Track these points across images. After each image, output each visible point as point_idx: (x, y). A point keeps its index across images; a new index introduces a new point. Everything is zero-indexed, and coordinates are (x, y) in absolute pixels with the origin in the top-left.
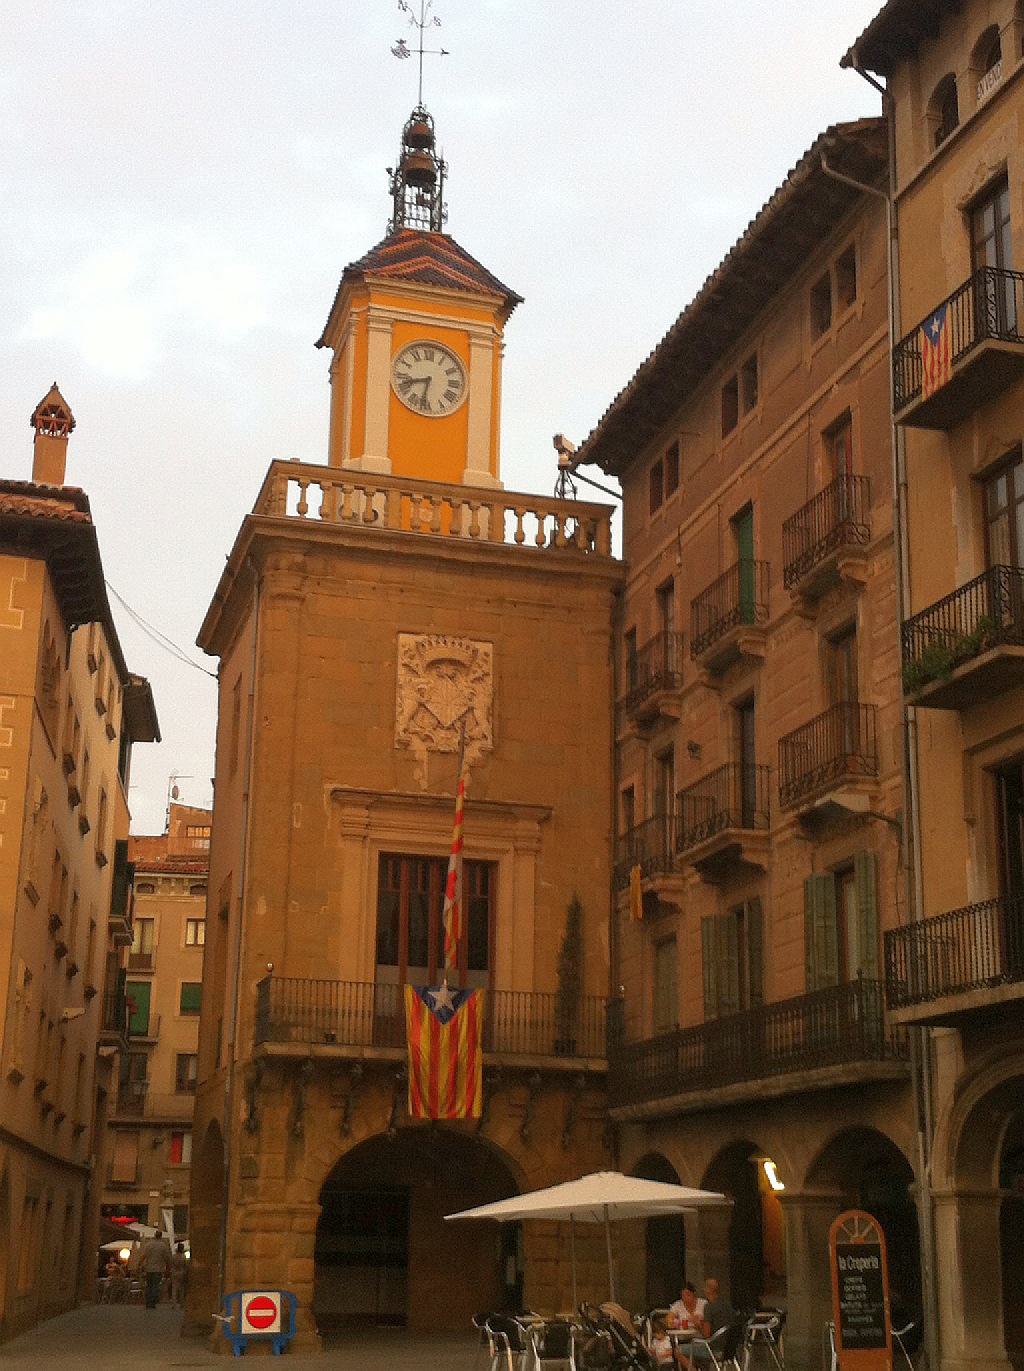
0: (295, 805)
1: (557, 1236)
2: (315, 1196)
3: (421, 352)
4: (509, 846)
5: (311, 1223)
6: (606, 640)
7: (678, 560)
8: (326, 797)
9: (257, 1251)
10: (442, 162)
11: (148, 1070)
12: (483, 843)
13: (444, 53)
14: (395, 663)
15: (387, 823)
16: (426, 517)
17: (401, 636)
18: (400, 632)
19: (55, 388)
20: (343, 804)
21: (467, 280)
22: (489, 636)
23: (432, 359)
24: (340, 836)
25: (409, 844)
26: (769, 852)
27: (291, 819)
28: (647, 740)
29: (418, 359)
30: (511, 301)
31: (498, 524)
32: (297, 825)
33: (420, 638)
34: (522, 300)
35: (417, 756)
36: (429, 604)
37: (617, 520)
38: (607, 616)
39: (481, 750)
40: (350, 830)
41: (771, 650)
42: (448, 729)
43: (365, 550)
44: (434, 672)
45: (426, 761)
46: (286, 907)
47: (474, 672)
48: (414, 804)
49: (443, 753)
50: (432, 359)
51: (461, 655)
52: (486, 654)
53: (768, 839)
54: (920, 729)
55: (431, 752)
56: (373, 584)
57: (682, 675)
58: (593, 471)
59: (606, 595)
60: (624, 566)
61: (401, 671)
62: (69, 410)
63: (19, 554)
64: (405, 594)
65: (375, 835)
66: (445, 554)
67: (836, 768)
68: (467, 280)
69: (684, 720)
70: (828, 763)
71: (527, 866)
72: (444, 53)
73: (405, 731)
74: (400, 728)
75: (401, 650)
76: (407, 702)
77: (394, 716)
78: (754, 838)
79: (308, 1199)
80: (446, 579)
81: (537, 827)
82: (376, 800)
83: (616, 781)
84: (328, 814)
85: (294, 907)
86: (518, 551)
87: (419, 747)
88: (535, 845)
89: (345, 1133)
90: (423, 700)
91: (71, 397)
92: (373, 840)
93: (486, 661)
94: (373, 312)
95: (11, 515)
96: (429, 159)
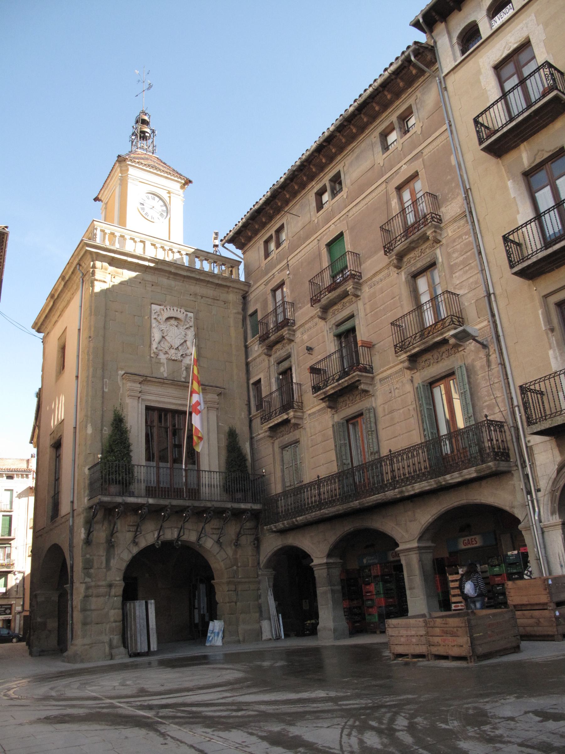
0: (105, 380)
1: (235, 591)
2: (122, 577)
6: (241, 317)
7: (288, 272)
11: (314, 146)
17: (153, 305)
18: (152, 304)
22: (192, 310)
25: (159, 402)
27: (103, 388)
28: (270, 356)
33: (162, 307)
35: (162, 361)
36: (165, 293)
37: (242, 267)
38: (241, 306)
40: (132, 394)
46: (102, 430)
48: (162, 382)
49: (174, 360)
51: (180, 316)
54: (498, 297)
55: (169, 360)
56: (139, 281)
58: (231, 246)
60: (247, 284)
61: (153, 321)
65: (144, 397)
66: (173, 270)
67: (421, 336)
70: (416, 334)
73: (156, 348)
74: (154, 346)
75: (153, 312)
76: (157, 336)
77: (151, 342)
79: (118, 579)
81: (217, 397)
82: (145, 380)
83: (248, 379)
84: (121, 386)
85: (105, 430)
87: (162, 357)
88: (217, 406)
89: (135, 542)
93: (191, 321)
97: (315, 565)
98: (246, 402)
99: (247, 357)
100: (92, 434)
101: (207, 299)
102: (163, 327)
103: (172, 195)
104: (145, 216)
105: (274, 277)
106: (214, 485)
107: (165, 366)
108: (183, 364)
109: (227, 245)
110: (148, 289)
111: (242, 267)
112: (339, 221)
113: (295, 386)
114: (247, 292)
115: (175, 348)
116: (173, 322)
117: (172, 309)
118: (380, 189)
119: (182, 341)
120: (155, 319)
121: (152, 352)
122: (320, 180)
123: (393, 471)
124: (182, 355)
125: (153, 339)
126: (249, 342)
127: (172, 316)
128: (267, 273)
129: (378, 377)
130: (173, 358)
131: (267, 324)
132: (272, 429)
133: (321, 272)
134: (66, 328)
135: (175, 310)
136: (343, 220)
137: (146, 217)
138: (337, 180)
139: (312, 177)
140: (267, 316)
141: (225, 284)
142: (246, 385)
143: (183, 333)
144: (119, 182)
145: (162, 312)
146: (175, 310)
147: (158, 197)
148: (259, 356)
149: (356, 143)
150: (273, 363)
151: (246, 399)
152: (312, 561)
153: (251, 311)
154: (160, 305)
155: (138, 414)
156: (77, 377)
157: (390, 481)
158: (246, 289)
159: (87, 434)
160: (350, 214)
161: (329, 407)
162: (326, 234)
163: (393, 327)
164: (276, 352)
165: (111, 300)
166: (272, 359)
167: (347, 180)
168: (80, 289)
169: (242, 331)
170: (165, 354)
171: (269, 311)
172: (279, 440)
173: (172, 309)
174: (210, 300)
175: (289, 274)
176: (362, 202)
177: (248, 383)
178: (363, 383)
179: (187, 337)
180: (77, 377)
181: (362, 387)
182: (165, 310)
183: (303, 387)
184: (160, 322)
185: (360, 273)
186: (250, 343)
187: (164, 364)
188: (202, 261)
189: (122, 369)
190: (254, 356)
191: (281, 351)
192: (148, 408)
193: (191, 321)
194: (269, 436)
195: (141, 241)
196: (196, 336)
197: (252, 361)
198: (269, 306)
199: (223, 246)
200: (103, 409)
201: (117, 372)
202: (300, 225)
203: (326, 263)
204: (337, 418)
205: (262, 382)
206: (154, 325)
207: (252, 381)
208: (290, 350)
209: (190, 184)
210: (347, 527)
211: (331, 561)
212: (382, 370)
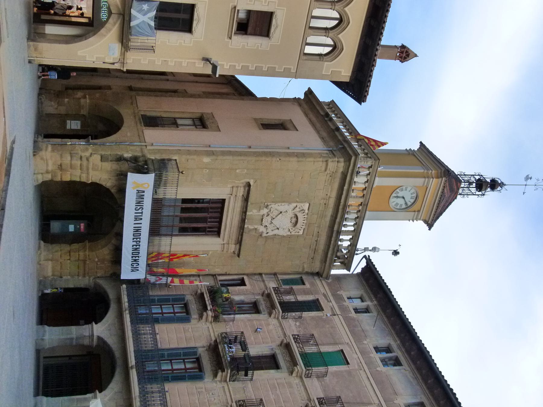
2: (94, 181)
3: (415, 195)
4: (225, 242)
5: (84, 180)
6: (301, 270)
7: (329, 315)
8: (248, 180)
9: (73, 162)
10: (484, 195)
12: (227, 233)
13: (524, 193)
14: (297, 202)
15: (237, 202)
16: (354, 202)
19: (416, 56)
20: (244, 187)
21: (439, 210)
23: (411, 198)
24: (233, 185)
26: (221, 381)
28: (263, 295)
29: (412, 194)
30: (430, 226)
31: (347, 233)
32: (238, 171)
33: (306, 211)
34: (430, 229)
35: (262, 211)
36: (319, 213)
37: (344, 272)
38: (309, 271)
39: (262, 232)
41: (295, 380)
42: (271, 222)
43: (342, 194)
44: (293, 216)
45: (260, 214)
46: (206, 168)
47: (292, 229)
50: (411, 198)
51: (299, 225)
52: (298, 232)
53: (226, 381)
56: (329, 194)
57: (287, 318)
58: (364, 264)
59: (317, 270)
60: (328, 276)
61: (294, 205)
62: (407, 61)
63: (353, 72)
64: (324, 205)
68: (439, 210)
69: (270, 320)
71: (218, 248)
72: (524, 193)
74: (273, 206)
75: (302, 204)
76: (283, 207)
78: (226, 377)
79: (93, 179)
80: (328, 219)
82: (246, 199)
83: (247, 275)
84: (241, 181)
85: (206, 171)
86: (338, 239)
90: (282, 213)
91: (412, 62)
92: (230, 198)
93: (296, 232)
94: (431, 179)
95: (368, 80)
96: (486, 189)
97: (92, 326)
101: (315, 245)
103: (416, 213)
104: (396, 191)
105: (328, 301)
106: (160, 248)
107: (258, 214)
108: (259, 226)
110: (322, 200)
111: (344, 272)
112: (359, 362)
113: (232, 316)
114: (322, 276)
116: (294, 220)
118: (375, 398)
122: (399, 348)
123: (152, 392)
128: (333, 295)
129: (225, 385)
131: (290, 293)
133: (317, 345)
135: (303, 222)
136: (359, 366)
137: (399, 189)
138: (397, 362)
139: (403, 342)
141: (328, 259)
142: (243, 273)
146: (303, 222)
147: (414, 202)
149: (421, 381)
151: (231, 273)
152: (96, 323)
157: (146, 390)
158: (324, 275)
160: (362, 372)
161: (210, 344)
162: (352, 350)
163: (259, 400)
165: (312, 174)
166: (259, 297)
167: (392, 371)
171: (297, 296)
174: (314, 247)
175: (327, 315)
176: (369, 382)
177: (244, 274)
178: (222, 374)
181: (220, 374)
183: (231, 323)
185: (310, 377)
188: (350, 240)
191: (264, 306)
192: (224, 200)
193: (296, 232)
195: (364, 195)
199: (365, 257)
201: (252, 179)
202: (367, 328)
203: (324, 349)
204: (201, 351)
207: (245, 278)
208: (263, 313)
209: (427, 228)
210: (117, 354)
211: (95, 338)
212: (231, 389)
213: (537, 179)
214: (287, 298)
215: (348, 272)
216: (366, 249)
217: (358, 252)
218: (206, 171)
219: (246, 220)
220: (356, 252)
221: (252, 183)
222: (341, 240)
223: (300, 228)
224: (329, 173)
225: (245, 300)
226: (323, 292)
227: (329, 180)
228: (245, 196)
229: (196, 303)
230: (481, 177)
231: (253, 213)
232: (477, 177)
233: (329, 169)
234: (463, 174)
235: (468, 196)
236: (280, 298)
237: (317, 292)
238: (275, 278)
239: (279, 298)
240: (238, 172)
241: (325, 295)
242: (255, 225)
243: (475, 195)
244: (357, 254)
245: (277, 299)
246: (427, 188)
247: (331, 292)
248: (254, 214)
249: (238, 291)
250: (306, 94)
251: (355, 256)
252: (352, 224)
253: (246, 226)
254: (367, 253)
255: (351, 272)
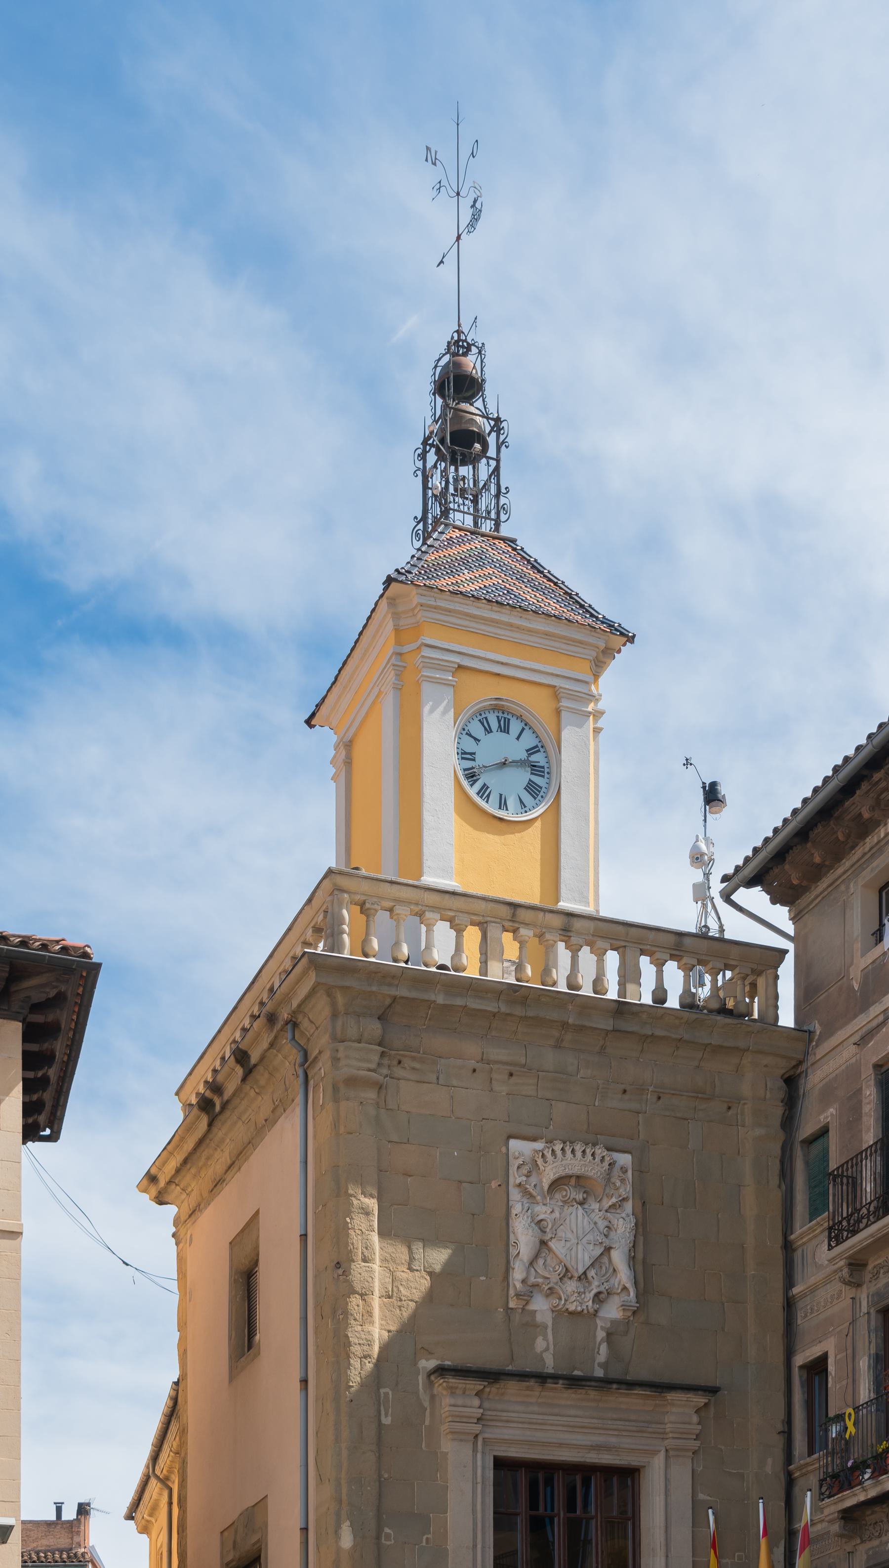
0: (382, 1391)
18: (510, 1137)
28: (859, 1285)
29: (489, 730)
32: (386, 1421)
33: (539, 1145)
37: (787, 971)
45: (550, 1324)
46: (378, 1538)
49: (572, 1313)
52: (624, 1170)
56: (472, 1064)
61: (515, 1195)
64: (514, 1078)
73: (524, 1281)
74: (518, 1274)
75: (514, 1164)
77: (508, 1262)
83: (789, 1354)
84: (426, 1404)
85: (388, 1537)
87: (540, 1306)
93: (623, 1181)
98: (780, 1427)
99: (789, 1281)
100: (354, 1547)
102: (542, 1211)
103: (564, 703)
108: (599, 1323)
109: (742, 896)
110: (496, 1087)
111: (787, 971)
115: (576, 1275)
117: (568, 1150)
119: (599, 1251)
120: (520, 1185)
121: (512, 1292)
124: (598, 1294)
125: (513, 1252)
126: (798, 1232)
127: (561, 1172)
130: (572, 1308)
131: (854, 1180)
132: (848, 1516)
134: (257, 1213)
135: (579, 1154)
140: (856, 1160)
142: (781, 1368)
143: (602, 1224)
144: (391, 676)
145: (540, 1161)
146: (579, 1154)
148: (827, 1281)
150: (864, 1309)
153: (807, 1129)
154: (534, 1139)
155: (475, 1484)
156: (304, 1382)
159: (339, 1550)
164: (876, 1276)
165: (394, 1137)
168: (299, 1099)
169: (776, 1196)
170: (547, 1296)
171: (865, 1146)
172: (869, 1545)
173: (568, 1150)
179: (612, 1234)
180: (304, 1382)
182: (549, 1155)
184: (531, 1196)
186: (801, 1236)
187: (546, 1328)
189: (429, 1353)
190: (812, 1280)
194: (841, 1536)
196: (641, 1227)
197: (804, 1295)
198: (865, 1119)
199: (727, 897)
200: (380, 1476)
205: (831, 1368)
206: (517, 1209)
207: (799, 1360)
213: (435, 192)
214: (868, 1190)
215: (790, 959)
216: (701, 893)
217: (713, 925)
218: (388, 1537)
219: (577, 1373)
220: (714, 932)
221: (432, 1364)
222: (660, 996)
223: (606, 1165)
224: (385, 1071)
225: (873, 1351)
226: (853, 1049)
227: (414, 1069)
228: (453, 1373)
229: (880, 1536)
230: (432, 445)
231: (547, 1349)
232: (432, 457)
233: (370, 1070)
234: (421, 526)
235: (503, 490)
236: (863, 1218)
237: (853, 1072)
238: (804, 1244)
239: (865, 1221)
240: (389, 1418)
241: (863, 1041)
242: (595, 1336)
243: (498, 460)
244: (722, 930)
245: (867, 1226)
246: (460, 667)
247: (855, 1016)
248: (552, 1347)
249: (845, 1382)
250: (160, 1200)
251: (728, 935)
252: (563, 954)
253: (599, 1373)
254: (717, 887)
255: (790, 946)
